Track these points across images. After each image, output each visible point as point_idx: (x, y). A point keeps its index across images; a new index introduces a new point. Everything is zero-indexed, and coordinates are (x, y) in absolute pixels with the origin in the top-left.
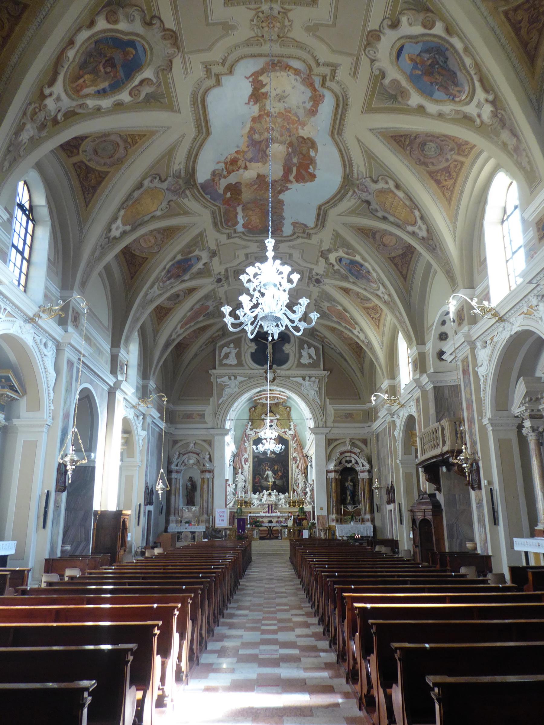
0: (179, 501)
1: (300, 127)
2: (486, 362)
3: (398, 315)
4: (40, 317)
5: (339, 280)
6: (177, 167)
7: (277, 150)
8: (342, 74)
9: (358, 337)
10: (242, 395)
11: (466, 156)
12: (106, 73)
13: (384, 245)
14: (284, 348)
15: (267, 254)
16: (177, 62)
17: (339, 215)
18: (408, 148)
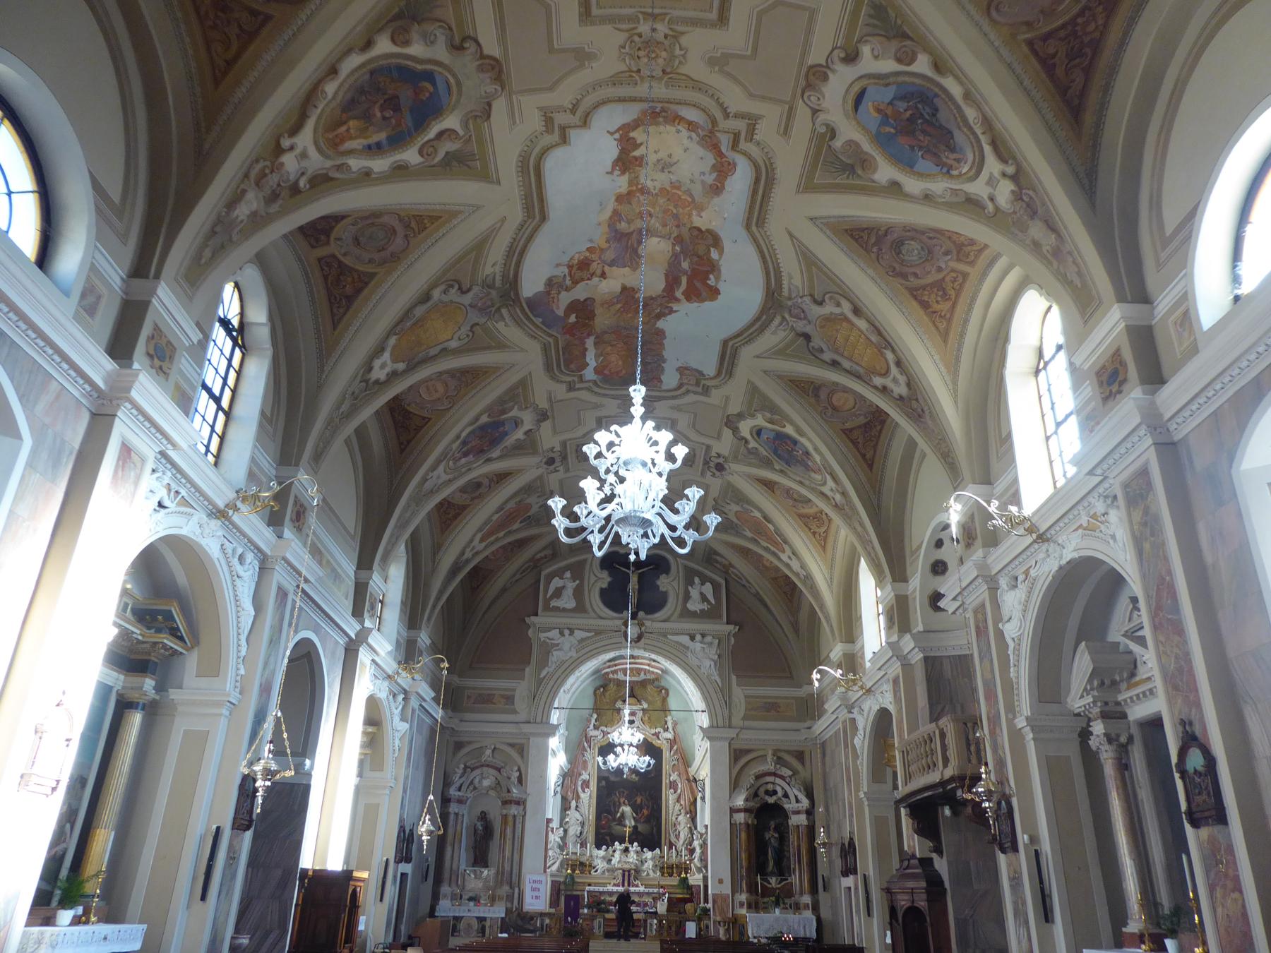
0: (460, 858)
1: (694, 213)
2: (1017, 615)
3: (859, 529)
4: (236, 509)
5: (759, 467)
6: (488, 270)
8: (765, 132)
9: (788, 566)
10: (582, 663)
11: (972, 263)
13: (834, 408)
14: (658, 583)
15: (632, 410)
16: (499, 106)
18: (875, 250)
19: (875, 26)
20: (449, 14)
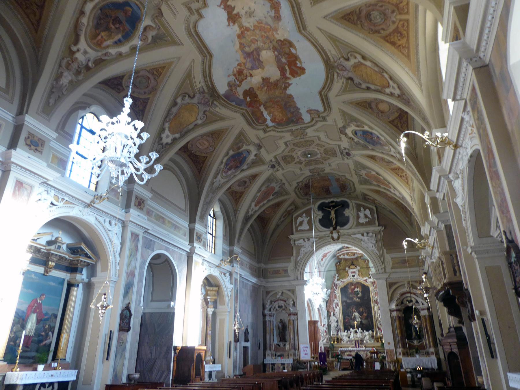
1: (274, 33)
3: (410, 169)
5: (362, 150)
6: (199, 86)
7: (267, 55)
9: (395, 194)
11: (407, 13)
12: (116, 28)
13: (382, 112)
14: (345, 213)
17: (337, 96)
18: (359, 22)
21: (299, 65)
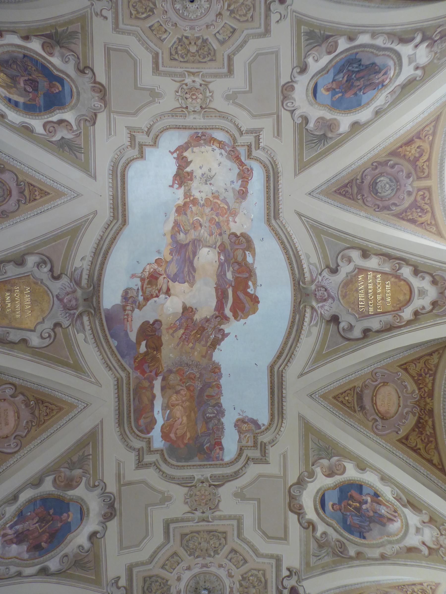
6: (78, 263)
7: (207, 258)
8: (266, 139)
11: (428, 177)
12: (25, 90)
16: (102, 118)
18: (359, 197)
19: (310, 44)
20: (79, 49)
21: (250, 291)
